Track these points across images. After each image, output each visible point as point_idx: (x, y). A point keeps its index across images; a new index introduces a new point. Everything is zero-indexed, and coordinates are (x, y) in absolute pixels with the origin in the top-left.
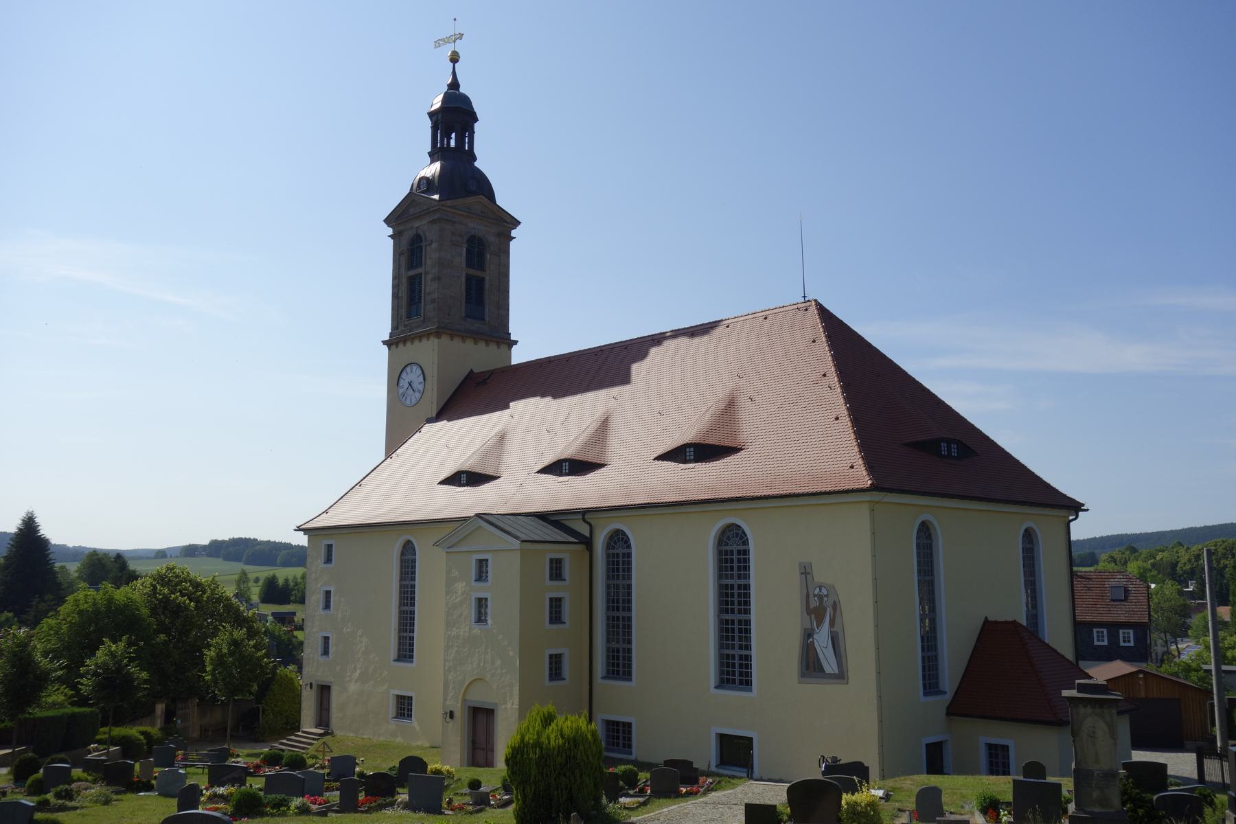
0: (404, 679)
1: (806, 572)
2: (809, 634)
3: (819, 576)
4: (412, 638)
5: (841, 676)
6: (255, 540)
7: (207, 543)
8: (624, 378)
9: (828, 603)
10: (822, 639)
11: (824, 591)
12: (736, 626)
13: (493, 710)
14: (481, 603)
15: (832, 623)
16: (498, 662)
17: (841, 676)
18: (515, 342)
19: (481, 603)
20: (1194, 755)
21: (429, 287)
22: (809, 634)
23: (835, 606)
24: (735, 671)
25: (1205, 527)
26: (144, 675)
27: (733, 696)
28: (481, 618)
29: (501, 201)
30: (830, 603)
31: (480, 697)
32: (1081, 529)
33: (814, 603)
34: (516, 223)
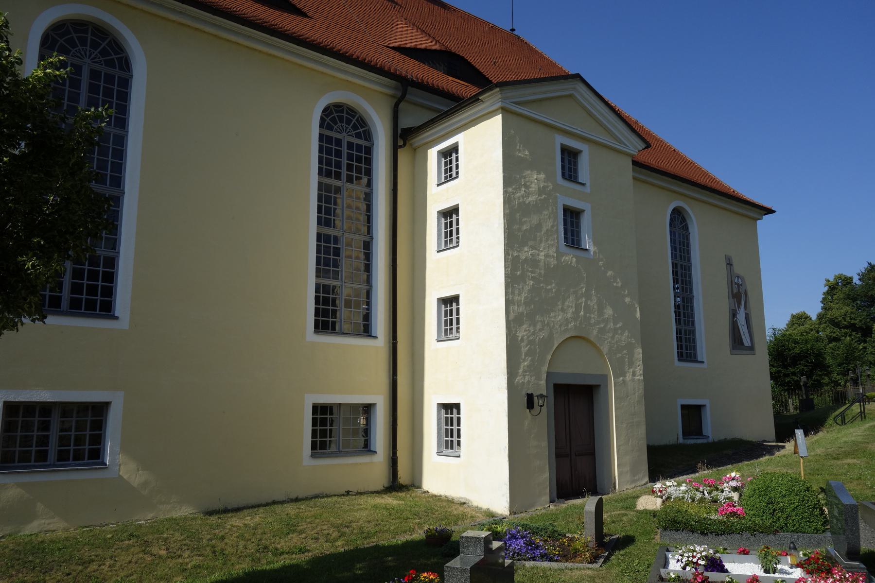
2: (734, 314)
14: (572, 216)
16: (609, 312)
19: (572, 216)
20: (306, 395)
22: (734, 314)
26: (674, 566)
28: (573, 238)
31: (577, 367)
33: (736, 290)
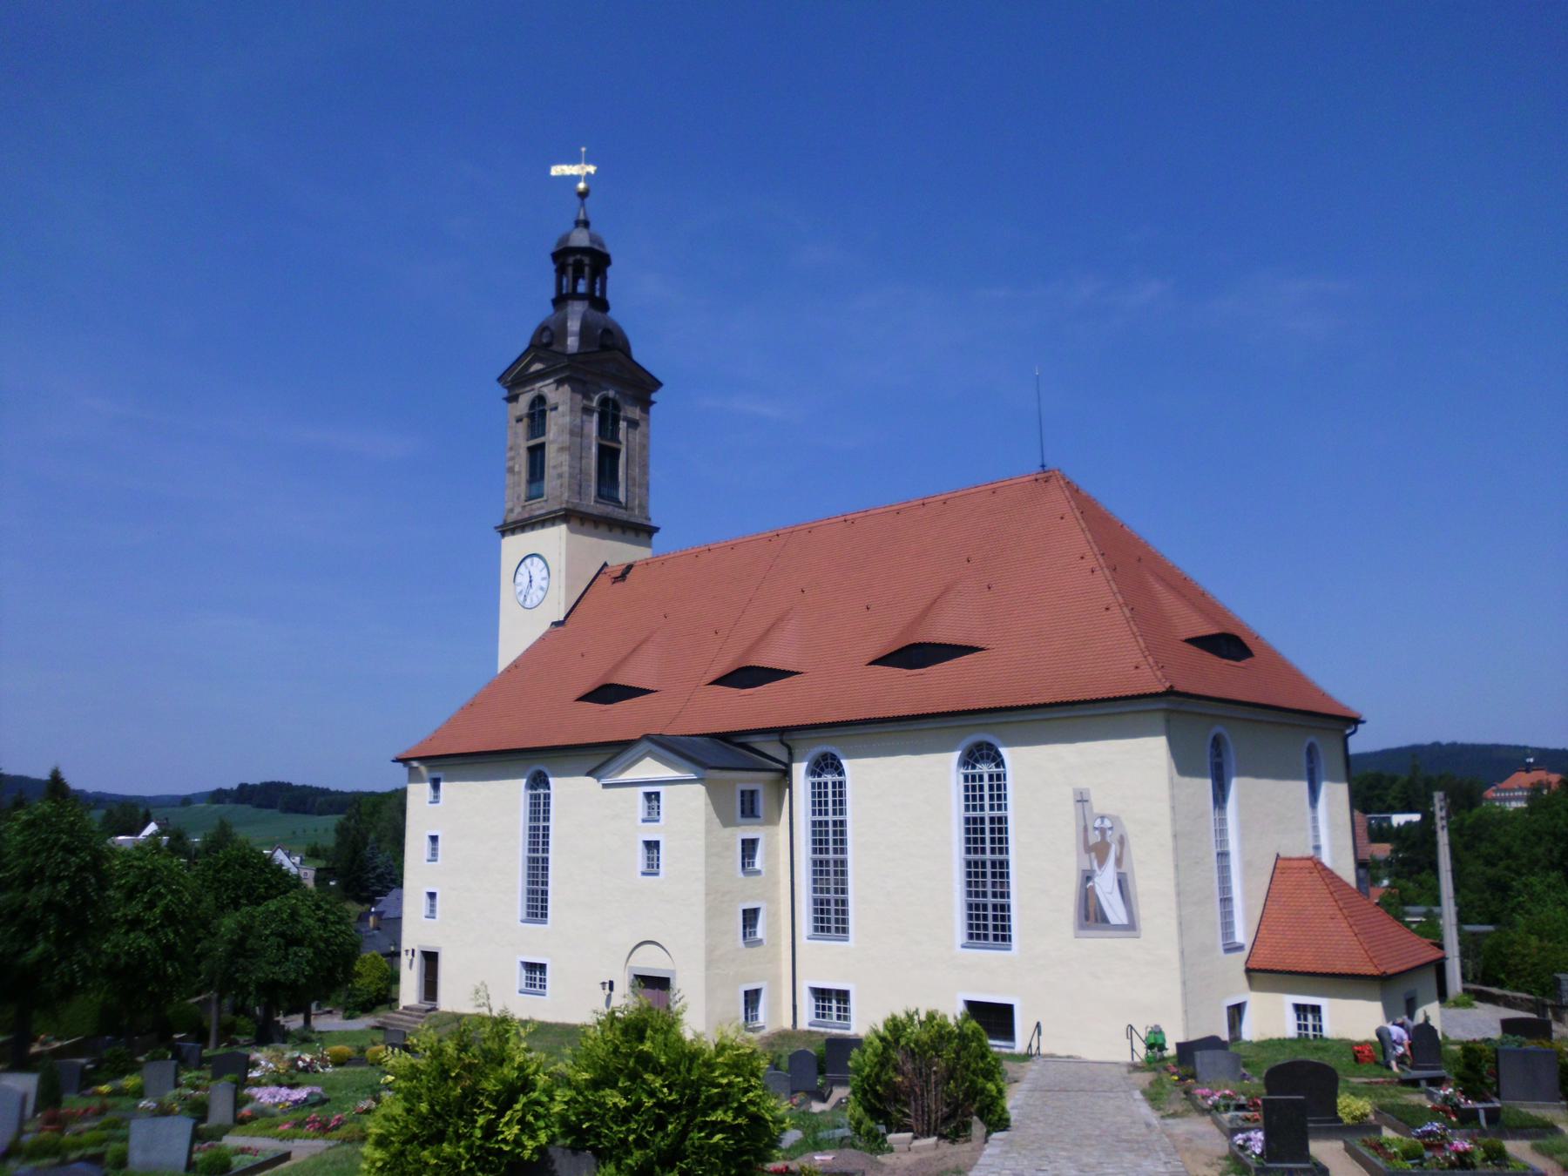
0: (537, 942)
1: (1082, 800)
2: (1088, 877)
3: (1099, 805)
4: (545, 893)
5: (1131, 927)
6: (289, 784)
7: (235, 787)
8: (243, 787)
9: (1112, 837)
10: (1105, 885)
11: (1107, 823)
12: (989, 870)
13: (667, 980)
15: (1119, 861)
17: (1131, 927)
18: (656, 529)
21: (555, 459)
22: (1088, 877)
23: (1122, 841)
24: (989, 921)
25: (1436, 746)
27: (987, 956)
28: (652, 868)
29: (638, 355)
30: (1117, 836)
31: (652, 962)
32: (1360, 743)
33: (1095, 838)
34: (657, 384)
